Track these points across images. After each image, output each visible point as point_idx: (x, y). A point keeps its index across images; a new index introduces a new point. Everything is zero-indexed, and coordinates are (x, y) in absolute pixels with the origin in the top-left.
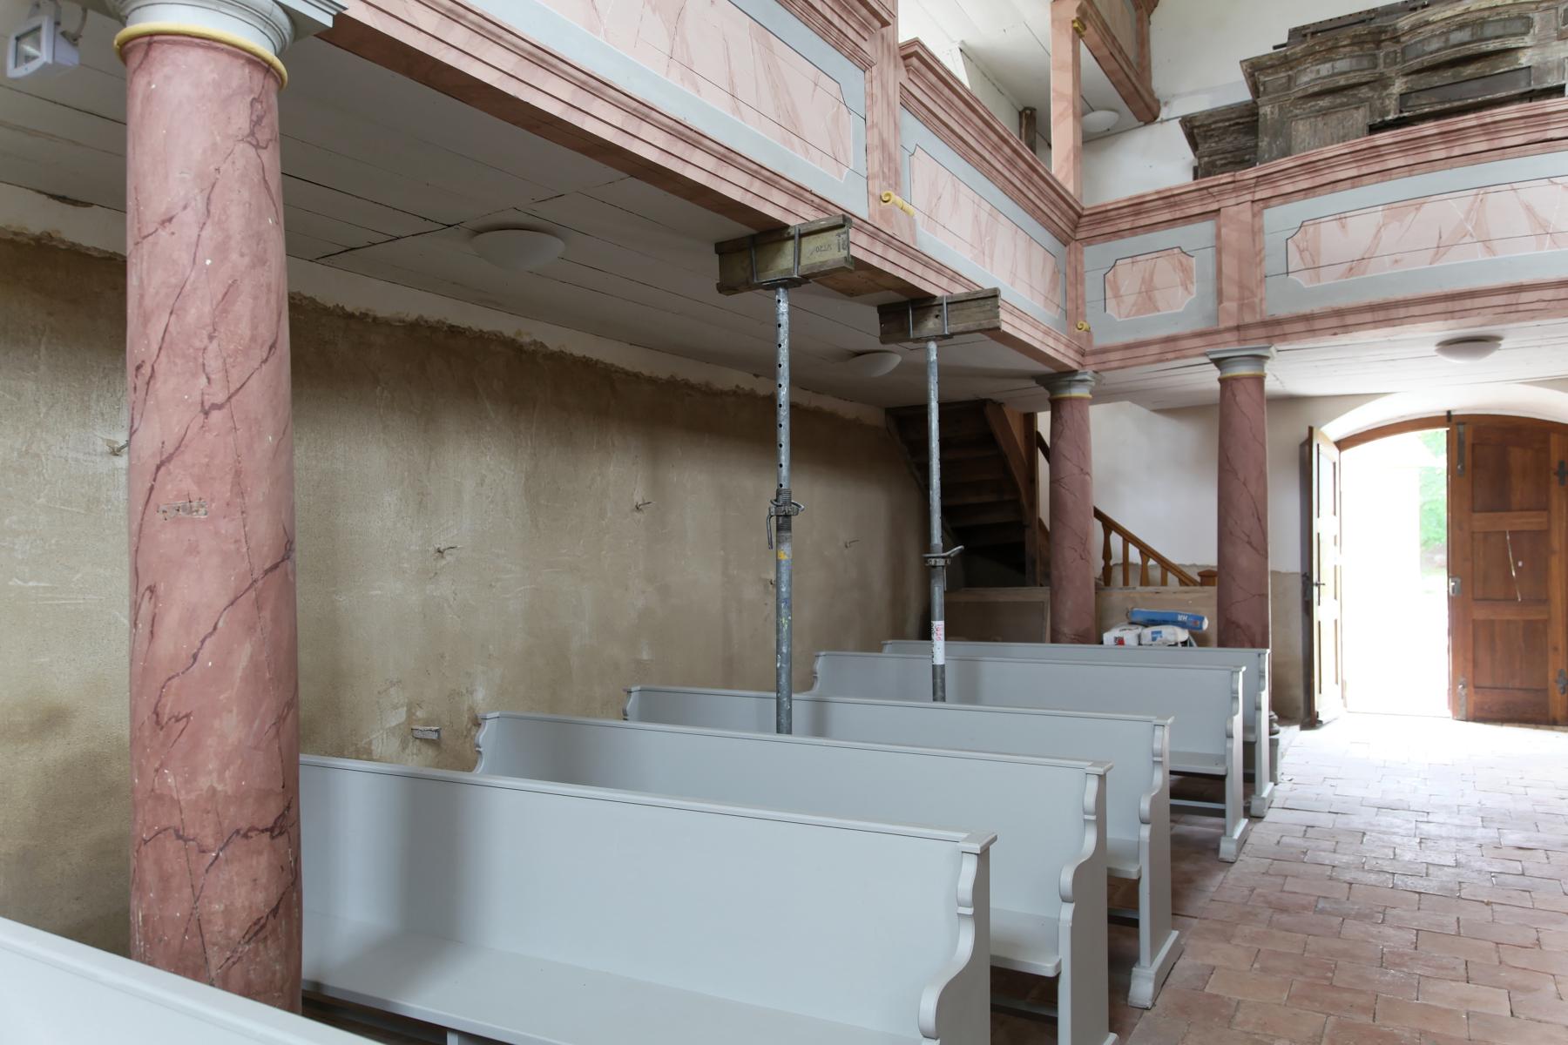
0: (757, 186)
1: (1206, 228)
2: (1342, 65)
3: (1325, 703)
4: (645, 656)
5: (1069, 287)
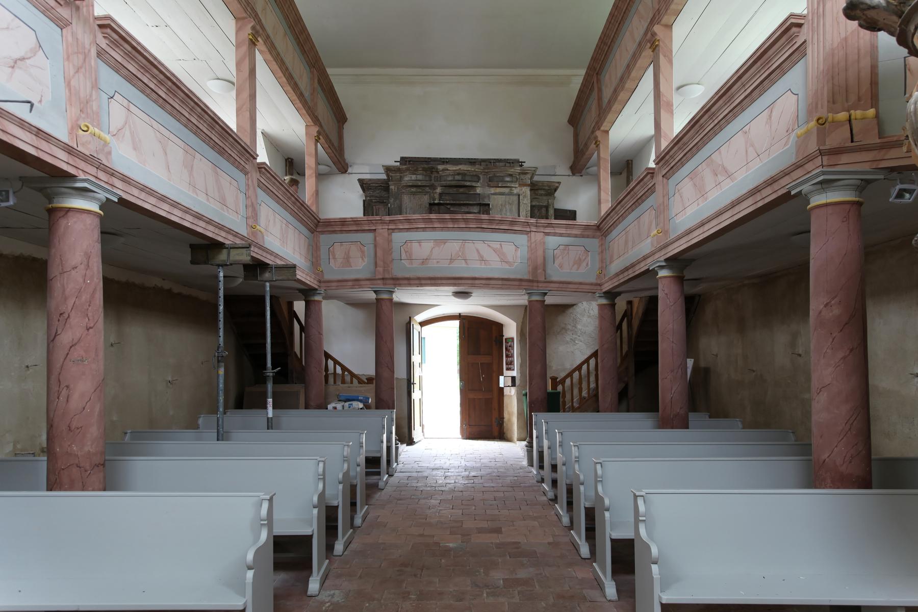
0: (217, 231)
1: (370, 236)
2: (420, 177)
3: (416, 434)
4: (115, 418)
5: (314, 253)
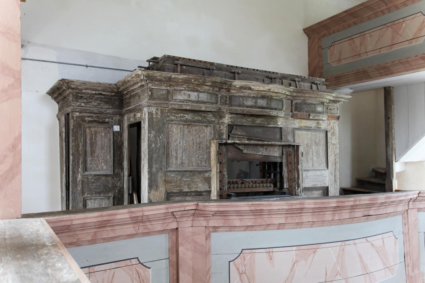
2: (203, 97)
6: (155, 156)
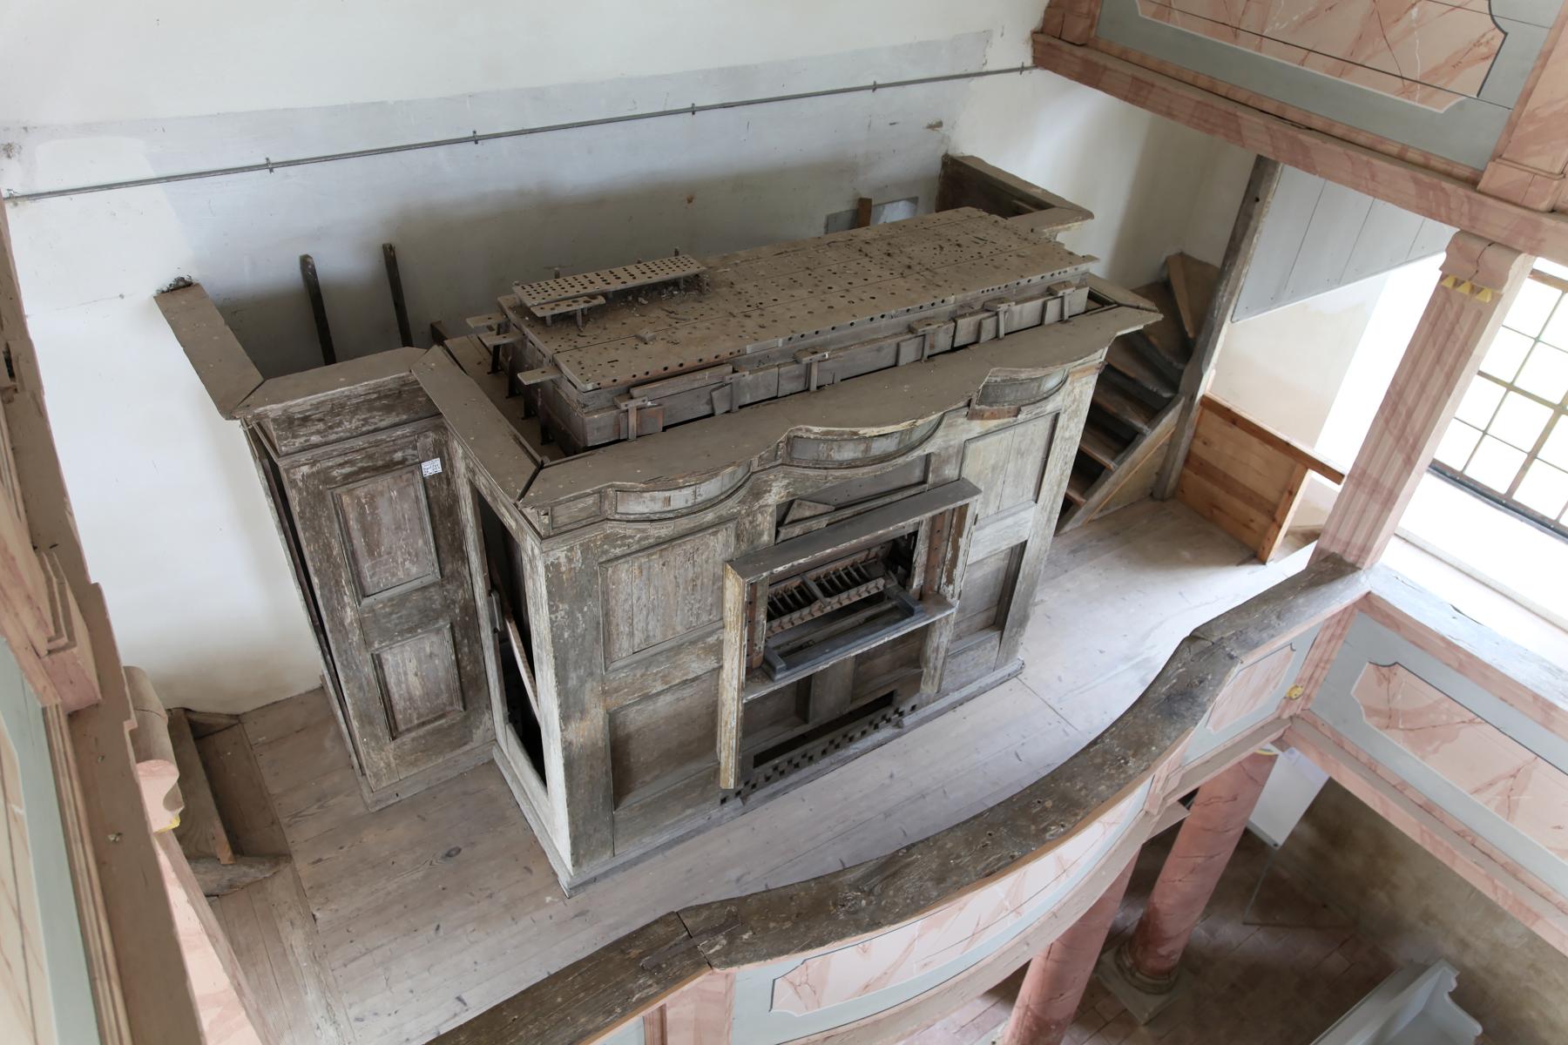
6: (572, 654)
